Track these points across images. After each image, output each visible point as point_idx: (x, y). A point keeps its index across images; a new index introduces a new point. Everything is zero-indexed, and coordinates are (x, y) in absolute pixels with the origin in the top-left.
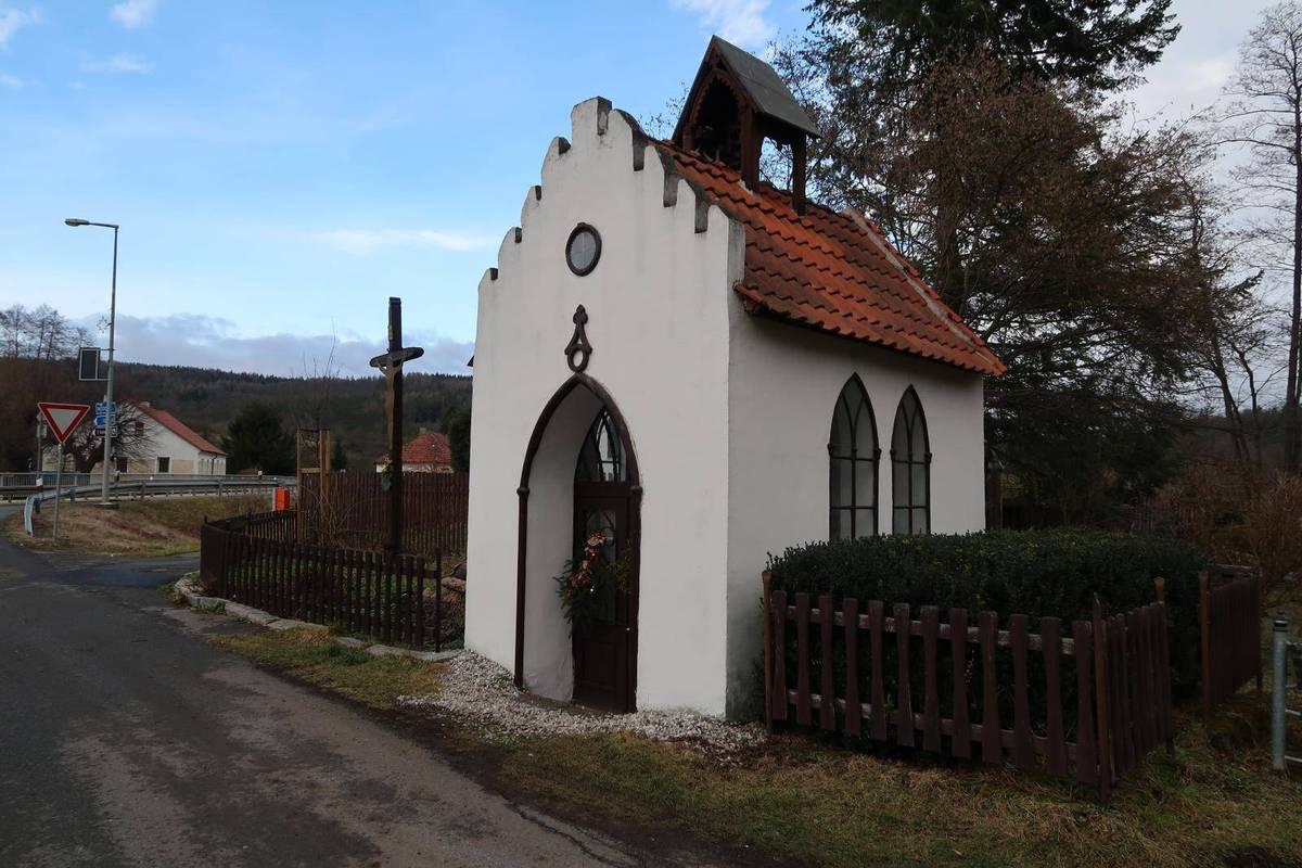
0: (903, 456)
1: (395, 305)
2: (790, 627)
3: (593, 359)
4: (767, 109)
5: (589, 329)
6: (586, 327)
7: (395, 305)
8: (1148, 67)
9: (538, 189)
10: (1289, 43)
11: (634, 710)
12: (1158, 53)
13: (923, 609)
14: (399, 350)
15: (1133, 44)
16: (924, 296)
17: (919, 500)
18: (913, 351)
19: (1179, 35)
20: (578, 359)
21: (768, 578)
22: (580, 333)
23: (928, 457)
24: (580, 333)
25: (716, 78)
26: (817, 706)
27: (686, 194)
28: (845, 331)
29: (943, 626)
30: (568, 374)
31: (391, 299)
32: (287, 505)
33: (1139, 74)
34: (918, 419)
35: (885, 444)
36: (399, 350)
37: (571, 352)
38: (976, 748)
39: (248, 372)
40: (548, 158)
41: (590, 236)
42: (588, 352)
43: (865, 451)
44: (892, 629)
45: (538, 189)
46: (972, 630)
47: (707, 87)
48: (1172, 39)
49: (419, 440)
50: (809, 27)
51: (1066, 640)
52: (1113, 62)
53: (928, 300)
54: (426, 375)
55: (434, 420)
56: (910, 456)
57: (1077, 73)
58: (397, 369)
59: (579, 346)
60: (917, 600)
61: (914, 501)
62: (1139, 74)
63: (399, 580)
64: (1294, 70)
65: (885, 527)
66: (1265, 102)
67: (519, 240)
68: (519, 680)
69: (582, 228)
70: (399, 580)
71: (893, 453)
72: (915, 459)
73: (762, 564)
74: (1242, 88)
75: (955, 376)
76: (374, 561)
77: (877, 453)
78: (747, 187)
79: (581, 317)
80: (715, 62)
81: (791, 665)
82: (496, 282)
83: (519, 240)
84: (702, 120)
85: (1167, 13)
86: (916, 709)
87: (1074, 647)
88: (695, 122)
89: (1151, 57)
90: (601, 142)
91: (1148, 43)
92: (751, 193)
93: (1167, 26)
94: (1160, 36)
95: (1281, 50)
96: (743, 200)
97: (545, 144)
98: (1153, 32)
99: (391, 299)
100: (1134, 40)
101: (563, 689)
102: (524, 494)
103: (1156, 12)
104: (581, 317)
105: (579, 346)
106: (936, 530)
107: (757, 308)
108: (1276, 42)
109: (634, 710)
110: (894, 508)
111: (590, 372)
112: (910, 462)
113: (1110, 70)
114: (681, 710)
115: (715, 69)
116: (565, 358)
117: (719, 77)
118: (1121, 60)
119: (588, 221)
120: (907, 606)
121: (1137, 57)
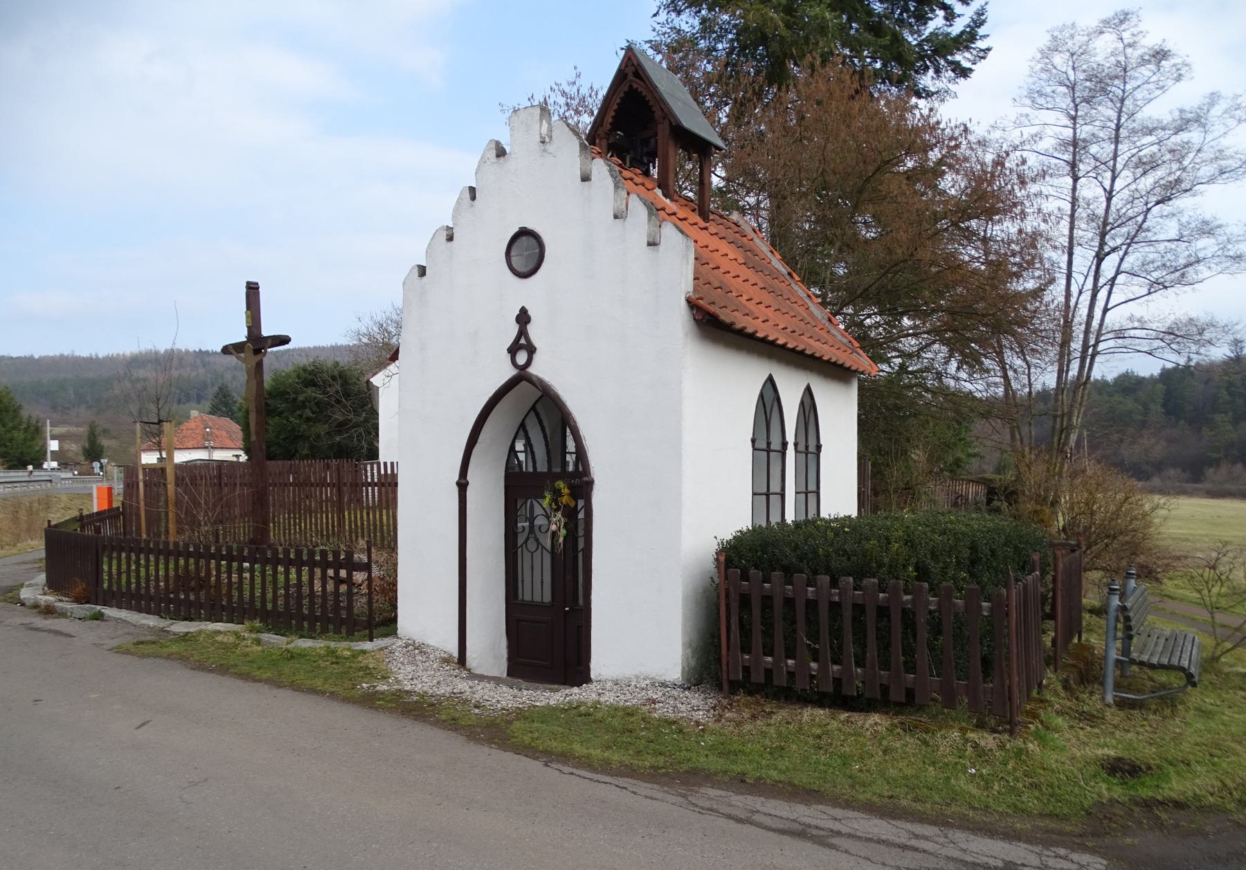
0: (802, 447)
1: (252, 290)
2: (745, 601)
3: (536, 357)
4: (686, 124)
5: (531, 329)
6: (529, 327)
7: (252, 290)
8: (961, 81)
9: (472, 190)
10: (1070, 63)
11: (588, 680)
12: (971, 70)
13: (865, 582)
14: (257, 343)
15: (949, 58)
16: (807, 300)
17: (812, 487)
18: (817, 355)
19: (990, 54)
20: (522, 358)
21: (722, 558)
22: (523, 332)
23: (819, 447)
24: (523, 332)
25: (631, 86)
26: (769, 666)
27: (638, 211)
28: (780, 342)
29: (881, 595)
30: (511, 372)
31: (248, 283)
32: (110, 502)
33: (952, 87)
34: (776, 408)
35: (790, 438)
36: (257, 343)
37: (513, 350)
38: (910, 694)
39: (66, 354)
40: (483, 161)
41: (532, 240)
42: (531, 350)
43: (776, 445)
44: (837, 599)
45: (472, 190)
46: (907, 598)
47: (622, 95)
48: (984, 58)
49: (192, 425)
50: (655, 15)
51: (984, 604)
52: (931, 72)
53: (810, 304)
54: (187, 352)
55: (199, 402)
56: (769, 444)
57: (899, 82)
58: (258, 358)
59: (522, 345)
60: (860, 573)
61: (810, 491)
62: (952, 87)
63: (287, 573)
64: (1073, 89)
65: (790, 517)
66: (1050, 117)
67: (450, 238)
68: (462, 660)
69: (524, 233)
70: (287, 573)
71: (796, 445)
72: (772, 447)
73: (714, 547)
74: (1028, 102)
75: (837, 372)
76: (305, 558)
77: (785, 445)
78: (664, 195)
79: (523, 318)
80: (630, 71)
81: (745, 631)
82: (424, 278)
83: (450, 238)
84: (615, 126)
85: (981, 31)
86: (858, 664)
87: (991, 610)
88: (609, 127)
89: (964, 73)
90: (544, 151)
91: (962, 58)
92: (668, 201)
93: (981, 44)
94: (974, 52)
95: (1064, 70)
96: (663, 209)
97: (482, 144)
98: (968, 48)
99: (248, 283)
100: (953, 52)
101: (501, 669)
102: (462, 486)
103: (972, 29)
104: (523, 318)
105: (522, 345)
106: (824, 514)
107: (707, 317)
108: (1059, 60)
109: (588, 680)
110: (754, 494)
111: (532, 370)
112: (768, 450)
113: (927, 80)
114: (637, 677)
115: (631, 77)
116: (507, 358)
117: (635, 86)
118: (938, 71)
119: (530, 226)
120: (851, 579)
121: (953, 70)
